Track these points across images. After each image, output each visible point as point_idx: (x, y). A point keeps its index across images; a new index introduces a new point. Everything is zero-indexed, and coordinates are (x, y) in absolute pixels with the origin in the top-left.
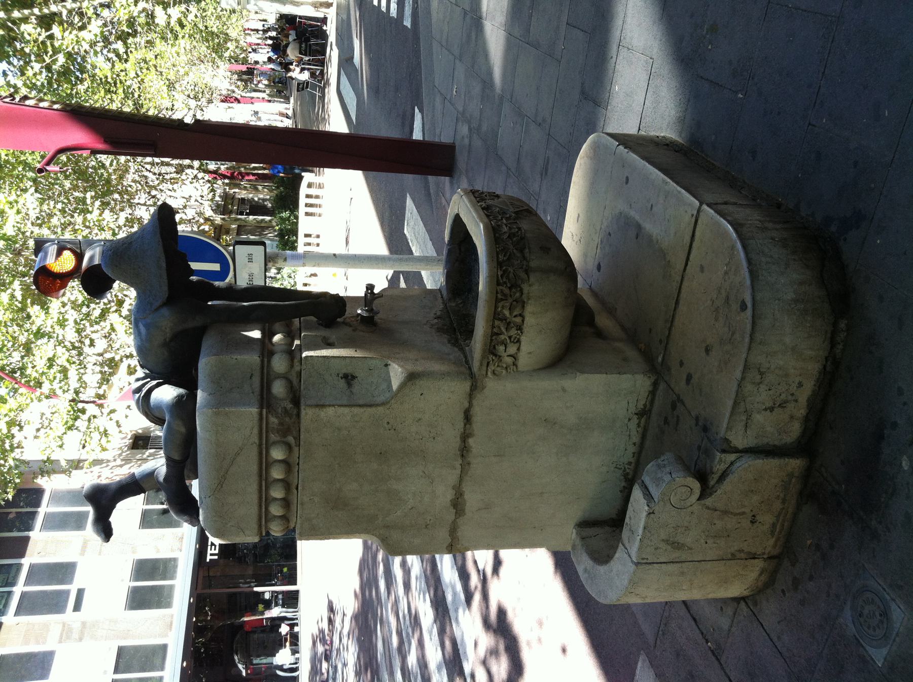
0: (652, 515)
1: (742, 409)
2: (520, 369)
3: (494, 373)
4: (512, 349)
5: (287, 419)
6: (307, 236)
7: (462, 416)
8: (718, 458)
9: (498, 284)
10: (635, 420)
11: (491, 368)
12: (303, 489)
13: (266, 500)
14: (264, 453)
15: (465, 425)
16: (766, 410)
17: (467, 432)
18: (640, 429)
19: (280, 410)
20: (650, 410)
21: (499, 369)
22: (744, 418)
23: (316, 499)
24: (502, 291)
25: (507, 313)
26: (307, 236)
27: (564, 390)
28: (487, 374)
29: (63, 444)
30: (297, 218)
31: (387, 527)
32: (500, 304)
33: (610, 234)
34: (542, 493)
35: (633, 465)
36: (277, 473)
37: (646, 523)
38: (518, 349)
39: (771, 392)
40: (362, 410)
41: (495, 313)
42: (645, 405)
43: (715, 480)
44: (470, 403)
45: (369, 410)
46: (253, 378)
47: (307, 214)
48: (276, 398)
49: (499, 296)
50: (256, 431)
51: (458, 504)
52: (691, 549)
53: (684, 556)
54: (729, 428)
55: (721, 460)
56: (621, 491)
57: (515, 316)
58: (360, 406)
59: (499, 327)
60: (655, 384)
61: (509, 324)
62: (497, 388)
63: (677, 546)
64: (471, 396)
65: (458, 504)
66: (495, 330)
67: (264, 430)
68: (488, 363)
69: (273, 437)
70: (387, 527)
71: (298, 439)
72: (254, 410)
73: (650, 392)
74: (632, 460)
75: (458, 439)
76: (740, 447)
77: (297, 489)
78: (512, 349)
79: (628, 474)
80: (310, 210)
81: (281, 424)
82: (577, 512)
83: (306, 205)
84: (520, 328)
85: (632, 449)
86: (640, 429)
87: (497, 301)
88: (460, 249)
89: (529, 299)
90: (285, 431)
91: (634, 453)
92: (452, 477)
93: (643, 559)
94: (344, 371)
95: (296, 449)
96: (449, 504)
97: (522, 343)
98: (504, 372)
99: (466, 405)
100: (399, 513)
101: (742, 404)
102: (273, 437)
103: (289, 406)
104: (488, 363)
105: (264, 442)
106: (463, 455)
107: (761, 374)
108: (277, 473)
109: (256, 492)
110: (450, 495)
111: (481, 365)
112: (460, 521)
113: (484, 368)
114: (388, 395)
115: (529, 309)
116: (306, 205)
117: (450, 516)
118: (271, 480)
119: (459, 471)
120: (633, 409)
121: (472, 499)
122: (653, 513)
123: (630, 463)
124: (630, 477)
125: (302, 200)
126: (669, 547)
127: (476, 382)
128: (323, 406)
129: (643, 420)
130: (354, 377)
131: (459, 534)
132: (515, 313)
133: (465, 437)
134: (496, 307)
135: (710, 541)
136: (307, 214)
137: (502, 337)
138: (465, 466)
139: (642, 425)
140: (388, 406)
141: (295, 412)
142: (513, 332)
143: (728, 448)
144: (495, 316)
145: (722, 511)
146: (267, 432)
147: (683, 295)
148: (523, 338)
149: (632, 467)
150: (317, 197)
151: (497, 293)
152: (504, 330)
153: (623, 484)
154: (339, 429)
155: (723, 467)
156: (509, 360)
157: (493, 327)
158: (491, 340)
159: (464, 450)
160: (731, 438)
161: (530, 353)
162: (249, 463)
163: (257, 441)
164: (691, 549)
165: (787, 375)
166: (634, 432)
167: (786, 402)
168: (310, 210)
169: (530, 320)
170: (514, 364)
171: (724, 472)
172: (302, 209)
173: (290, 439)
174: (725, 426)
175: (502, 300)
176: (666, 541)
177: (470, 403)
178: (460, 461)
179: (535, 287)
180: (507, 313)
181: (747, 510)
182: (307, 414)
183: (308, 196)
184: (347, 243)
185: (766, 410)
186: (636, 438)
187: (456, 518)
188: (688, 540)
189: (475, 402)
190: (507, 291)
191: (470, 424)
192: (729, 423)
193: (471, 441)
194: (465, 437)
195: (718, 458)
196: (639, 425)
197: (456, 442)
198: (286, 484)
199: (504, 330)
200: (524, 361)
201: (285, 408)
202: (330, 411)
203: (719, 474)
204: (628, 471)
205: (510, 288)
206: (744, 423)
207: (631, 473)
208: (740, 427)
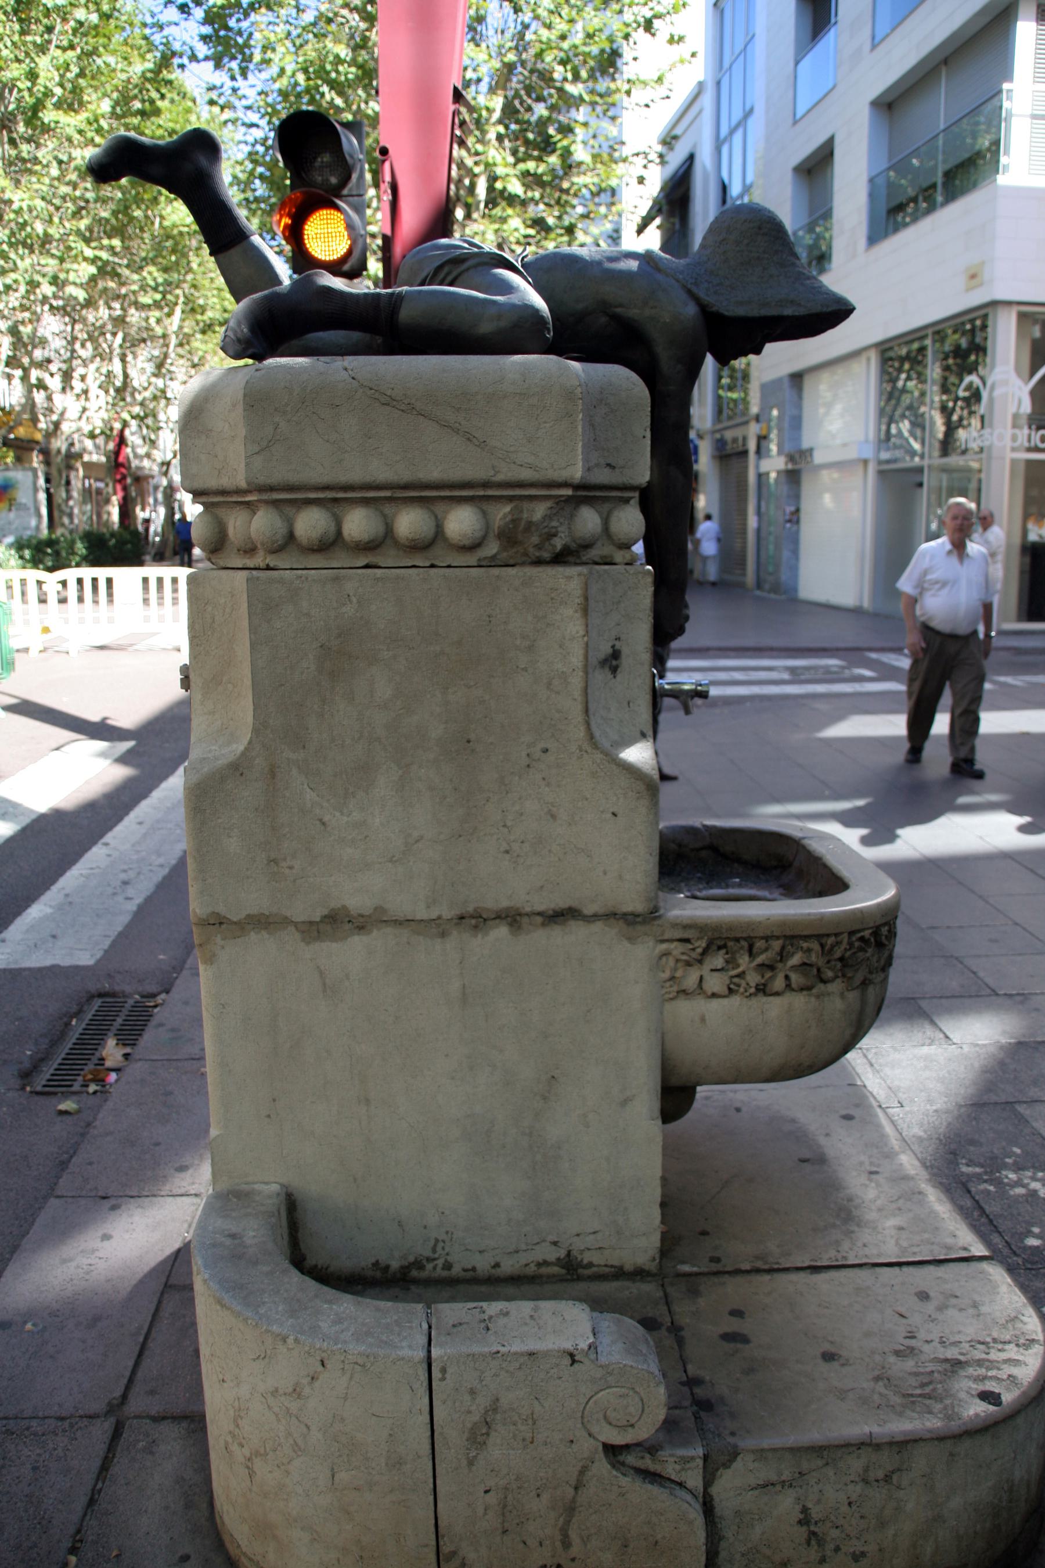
0: (567, 1361)
1: (805, 1466)
2: (668, 1006)
3: (666, 954)
4: (715, 983)
5: (535, 539)
6: (109, 581)
7: (562, 903)
8: (689, 1452)
9: (851, 933)
10: (552, 1254)
11: (677, 949)
12: (377, 579)
13: (335, 500)
14: (443, 494)
15: (539, 914)
16: (805, 1510)
17: (525, 920)
18: (533, 1267)
19: (554, 524)
20: (580, 1278)
21: (671, 962)
22: (786, 1475)
23: (349, 610)
24: (838, 943)
25: (796, 960)
26: (109, 581)
27: (625, 1102)
28: (663, 941)
29: (198, 61)
30: (78, 565)
31: (272, 772)
32: (815, 946)
33: (738, 1110)
34: (367, 1101)
35: (445, 1273)
36: (409, 522)
37: (547, 1354)
38: (714, 995)
39: (845, 1508)
40: (578, 694)
41: (793, 937)
42: (590, 1265)
43: (640, 1464)
44: (595, 917)
45: (579, 708)
46: (607, 470)
47: (145, 580)
48: (572, 516)
49: (831, 941)
50: (526, 475)
51: (337, 923)
52: (471, 1463)
53: (449, 1456)
54: (761, 1454)
55: (686, 1460)
56: (376, 1264)
57: (787, 977)
58: (586, 689)
59: (766, 950)
60: (639, 1274)
61: (771, 967)
62: (630, 968)
63: (478, 1436)
64: (611, 916)
65: (337, 923)
66: (760, 944)
67: (517, 492)
68: (687, 941)
69: (501, 513)
70: (272, 772)
71: (492, 563)
72: (577, 473)
73: (621, 1268)
74: (456, 1270)
75: (505, 903)
76: (714, 1490)
77: (367, 567)
78: (715, 983)
79: (421, 1267)
80: (153, 585)
81: (530, 524)
82: (321, 1181)
83: (95, 580)
84: (762, 990)
85: (482, 1264)
86: (533, 1267)
87: (818, 937)
88: (702, 849)
89: (818, 997)
90: (509, 536)
91: (474, 1269)
92: (409, 902)
93: (444, 1370)
94: (625, 651)
95: (472, 559)
96: (334, 904)
97: (725, 1002)
98: (667, 975)
99: (588, 910)
100: (310, 795)
101: (820, 1462)
102: (501, 513)
103: (558, 543)
104: (687, 941)
105: (490, 492)
106: (462, 918)
107: (887, 1478)
108: (409, 522)
109: (368, 479)
110: (357, 902)
111: (686, 927)
112: (291, 937)
113: (679, 934)
114: (606, 744)
115: (799, 1001)
116: (95, 580)
117: (302, 910)
118: (439, 508)
119: (422, 914)
120: (578, 1244)
121: (350, 953)
122: (574, 1362)
123: (448, 1266)
124: (414, 1273)
125: (102, 573)
126: (476, 1417)
127: (644, 922)
128: (585, 611)
129: (556, 1270)
130: (614, 670)
131: (253, 936)
132: (794, 977)
133: (513, 918)
134: (806, 938)
135: (492, 1499)
136: (145, 580)
137: (744, 960)
138: (436, 928)
139: (544, 1270)
140: (586, 746)
141: (546, 555)
142: (753, 979)
143: (710, 1470)
144: (791, 936)
145: (574, 1500)
146: (511, 499)
147: (776, 1275)
148: (736, 1000)
149: (440, 1272)
150: (161, 598)
151: (836, 935)
152: (760, 960)
153: (395, 1265)
154: (530, 648)
155: (670, 1470)
156: (691, 980)
157: (767, 938)
158: (737, 940)
159: (476, 920)
160: (738, 1464)
161: (703, 1020)
162: (443, 460)
163: (500, 478)
164: (471, 1463)
165: (882, 1524)
166: (523, 1258)
167: (821, 1542)
168: (153, 585)
169: (774, 1007)
170: (684, 992)
171: (660, 1476)
172: (87, 573)
173: (492, 548)
174: (766, 1444)
175: (822, 946)
176: (494, 1407)
177: (595, 917)
178: (447, 914)
179: (838, 1004)
180: (796, 960)
181: (575, 1550)
182: (568, 580)
183: (160, 581)
184: (102, 648)
185: (805, 1510)
186: (509, 1266)
187: (296, 924)
188: (496, 1450)
189: (598, 926)
190: (838, 953)
191: (543, 925)
192: (775, 1450)
193: (501, 931)
194: (513, 918)
195: (689, 1452)
196: (545, 1263)
197: (495, 899)
198: (330, 544)
199: (760, 960)
200: (686, 1010)
201: (555, 535)
202: (575, 627)
203: (653, 1467)
204: (429, 1266)
205: (841, 959)
206: (774, 1478)
207: (424, 1274)
208: (765, 1473)
